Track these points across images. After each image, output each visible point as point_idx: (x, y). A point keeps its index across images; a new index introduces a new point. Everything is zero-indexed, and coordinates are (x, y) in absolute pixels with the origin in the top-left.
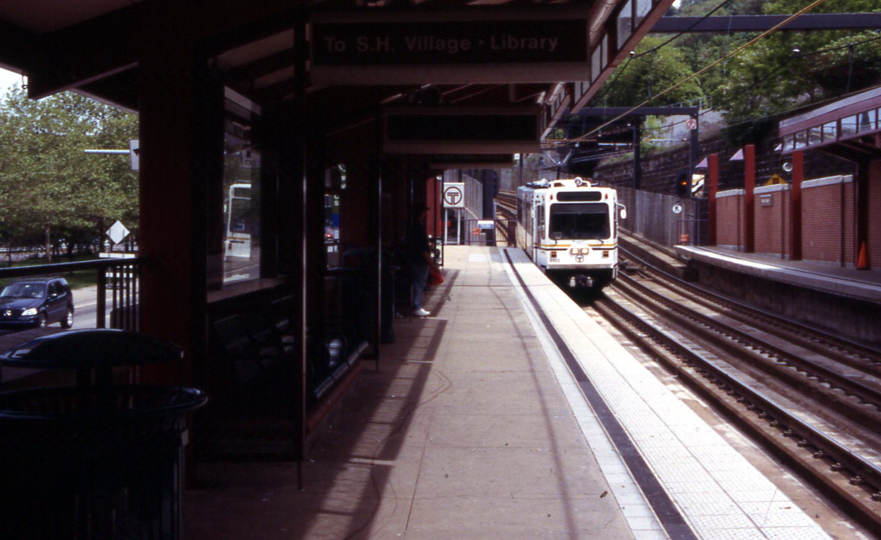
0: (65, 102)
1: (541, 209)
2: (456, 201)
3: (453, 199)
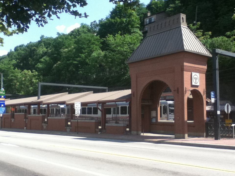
0: (109, 56)
1: (53, 110)
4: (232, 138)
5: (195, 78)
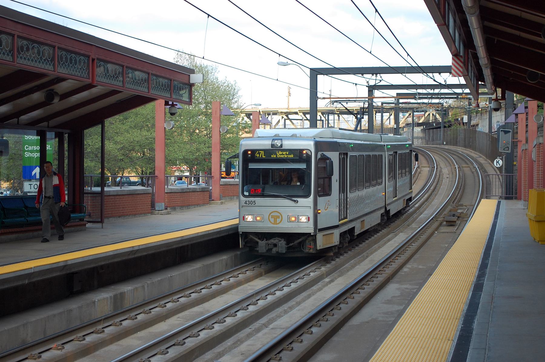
2: (277, 223)
5: (271, 216)
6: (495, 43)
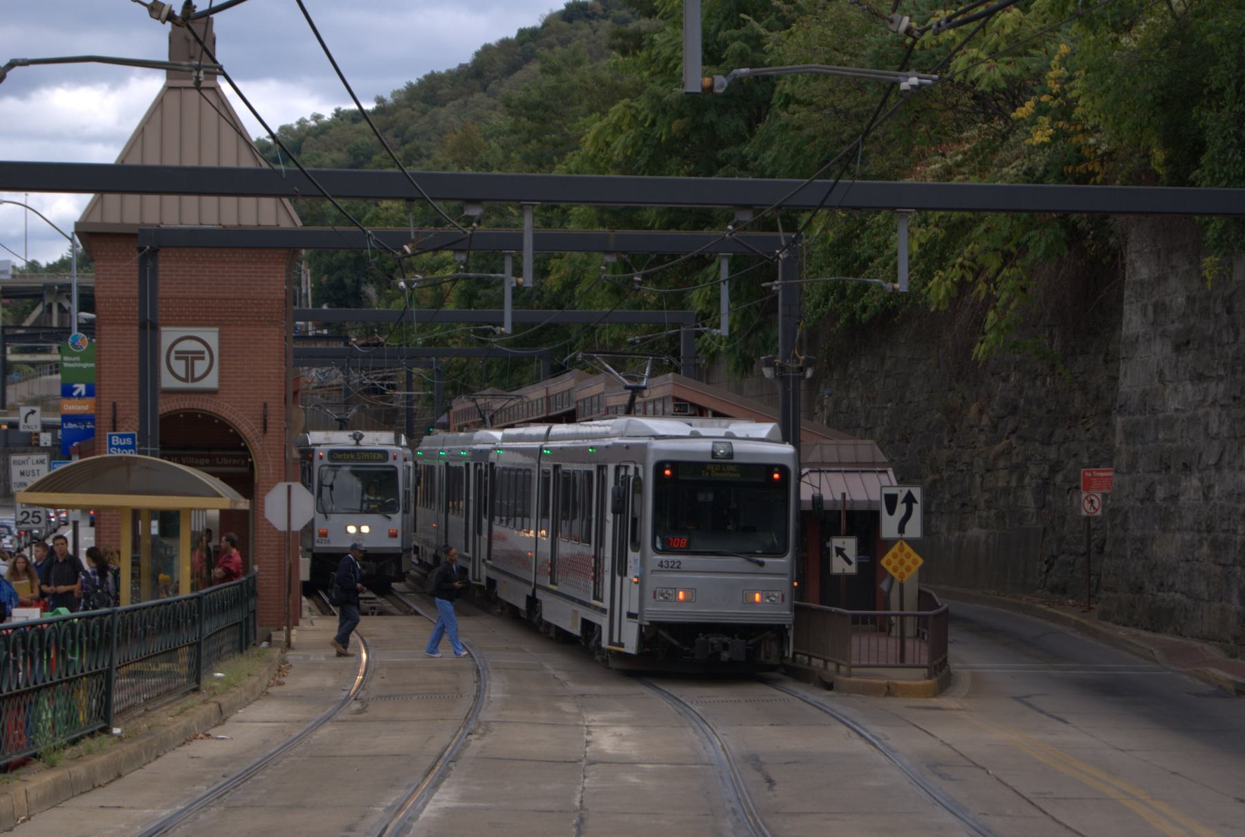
2: (197, 375)
3: (190, 368)
4: (676, 465)
5: (177, 352)
6: (763, 285)
